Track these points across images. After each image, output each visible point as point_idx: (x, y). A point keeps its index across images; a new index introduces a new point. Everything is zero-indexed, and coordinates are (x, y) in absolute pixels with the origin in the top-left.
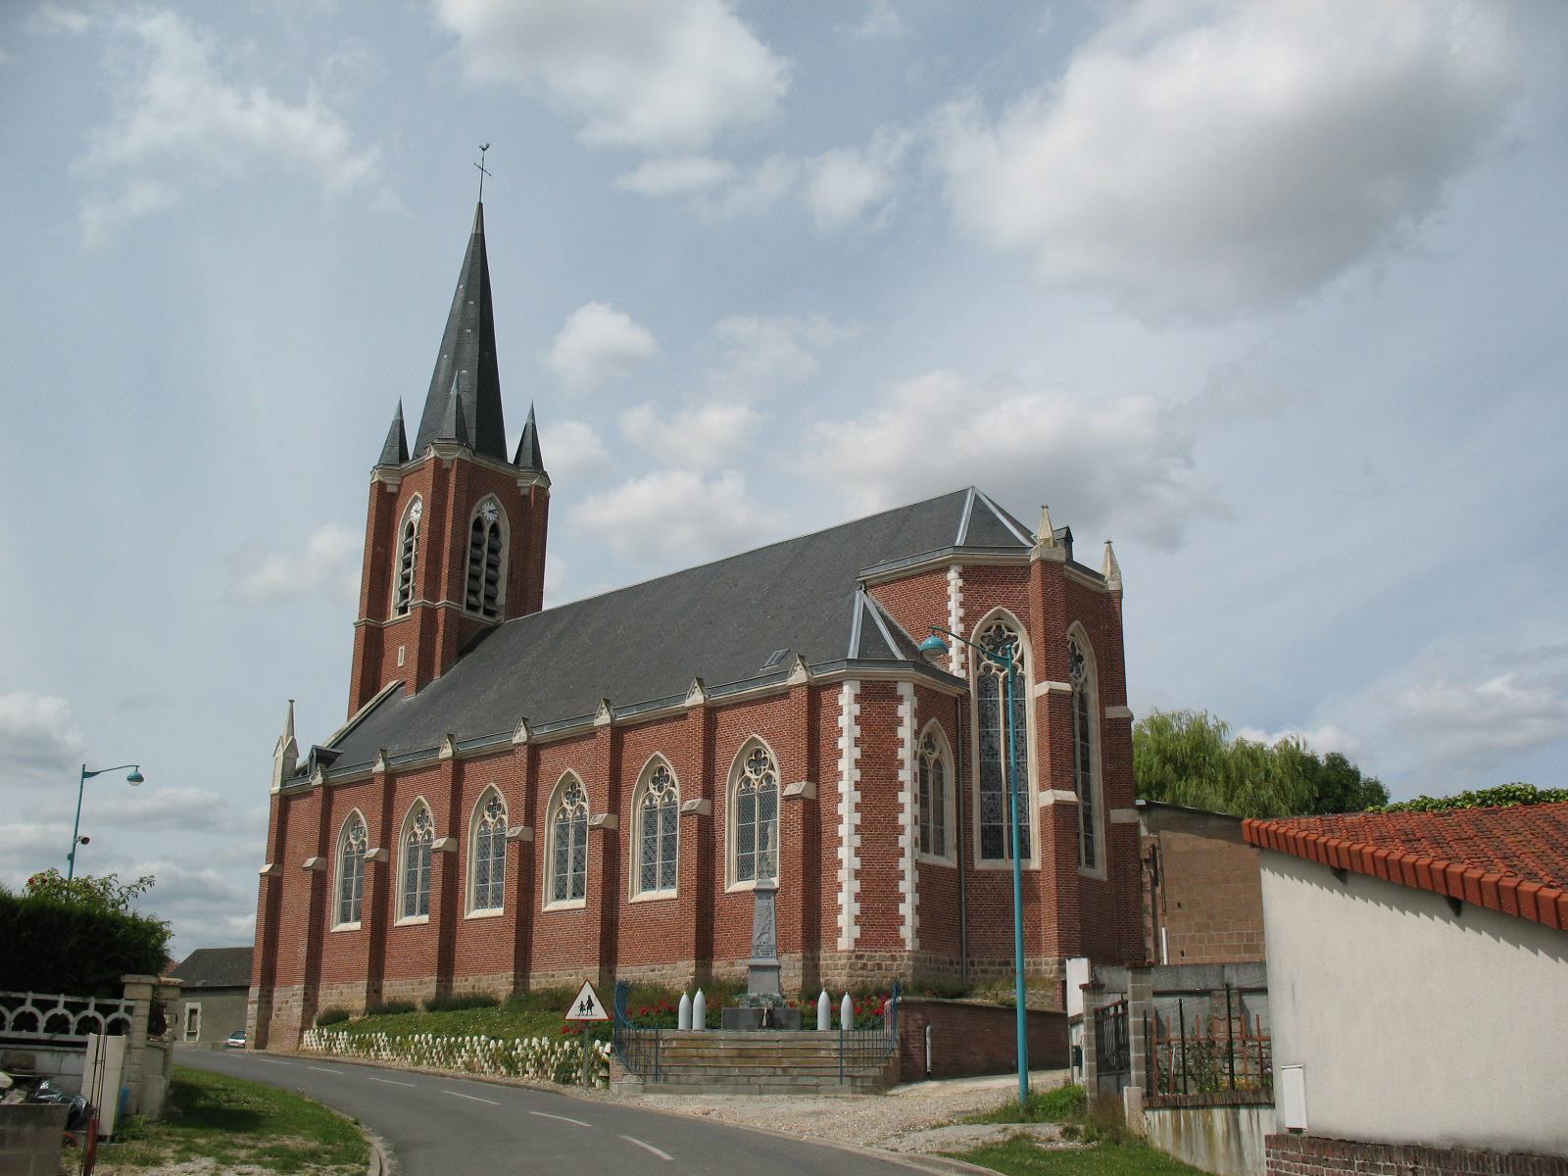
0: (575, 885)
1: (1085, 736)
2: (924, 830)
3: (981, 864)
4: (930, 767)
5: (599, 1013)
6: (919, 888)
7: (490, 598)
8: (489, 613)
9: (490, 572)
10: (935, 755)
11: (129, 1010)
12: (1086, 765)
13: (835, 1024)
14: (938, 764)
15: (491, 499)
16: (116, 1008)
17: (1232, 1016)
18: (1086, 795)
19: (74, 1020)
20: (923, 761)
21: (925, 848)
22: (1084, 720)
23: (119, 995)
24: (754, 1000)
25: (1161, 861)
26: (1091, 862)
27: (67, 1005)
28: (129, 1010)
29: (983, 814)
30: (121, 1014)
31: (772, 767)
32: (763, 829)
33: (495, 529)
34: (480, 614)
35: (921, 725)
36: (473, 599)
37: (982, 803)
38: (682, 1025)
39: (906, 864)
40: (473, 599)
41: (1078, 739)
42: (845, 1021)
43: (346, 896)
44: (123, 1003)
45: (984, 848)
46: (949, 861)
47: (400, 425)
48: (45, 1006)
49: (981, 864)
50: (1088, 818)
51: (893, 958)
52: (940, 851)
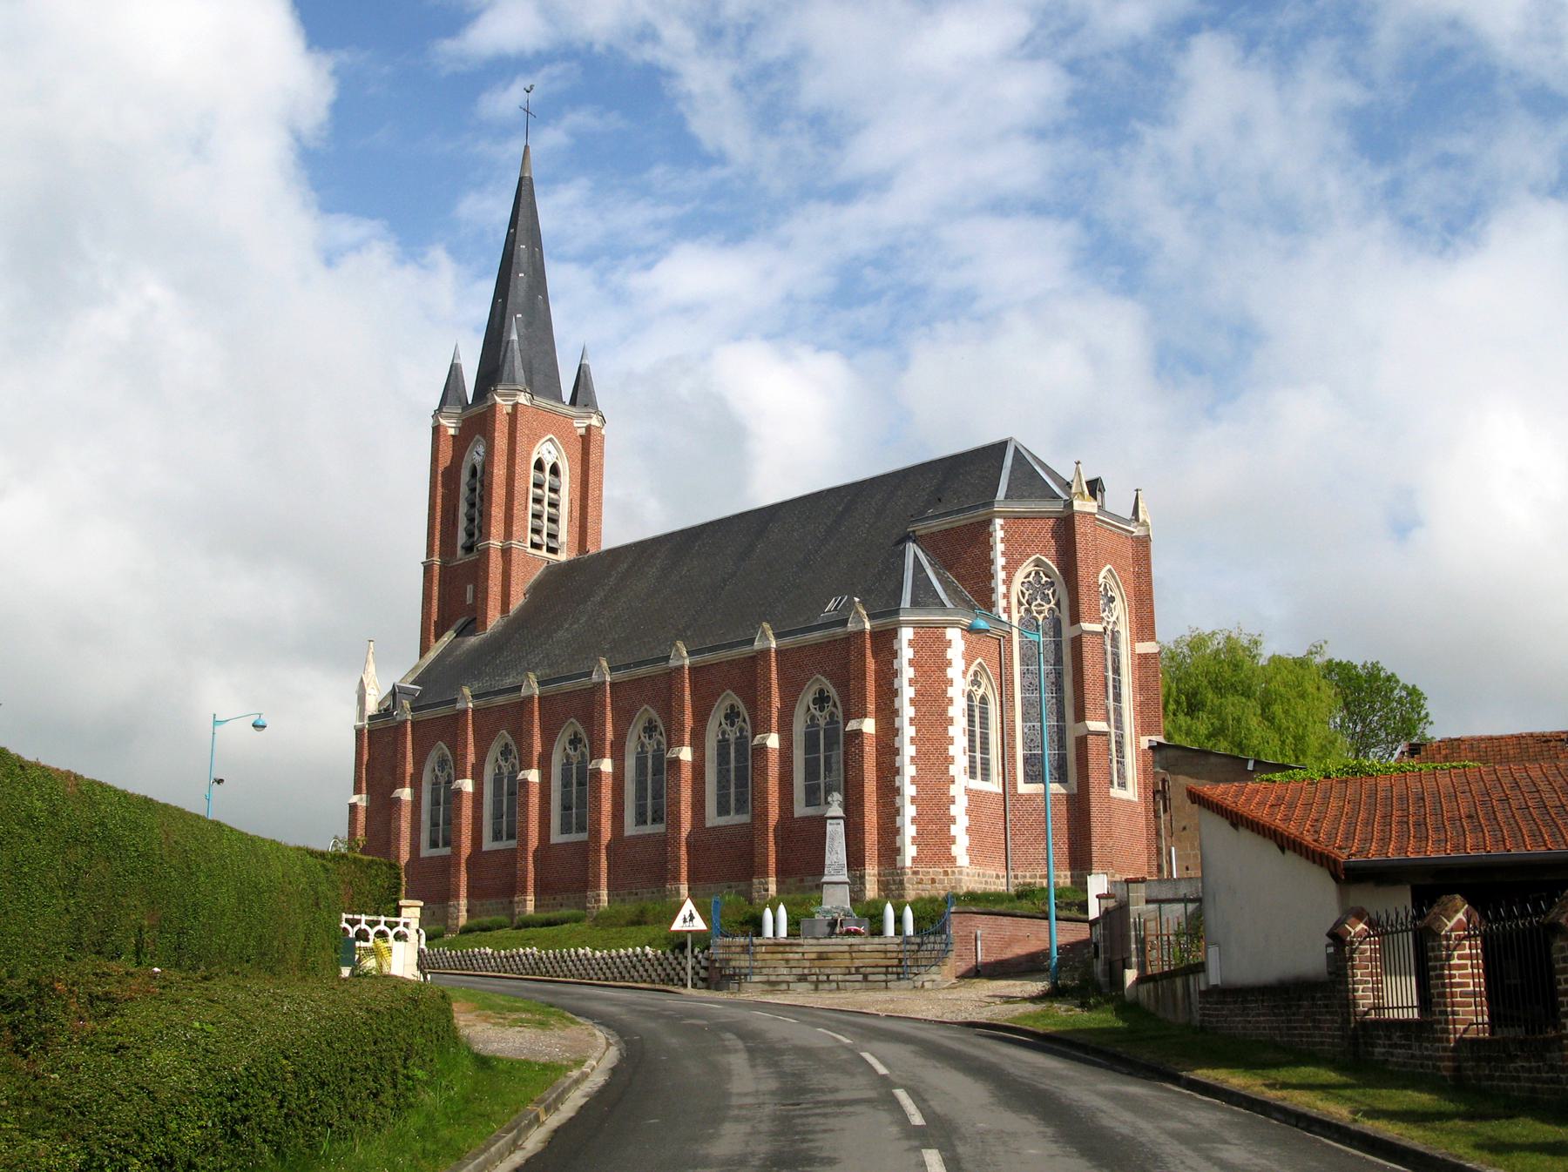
0: (655, 812)
1: (1117, 671)
2: (972, 760)
3: (1024, 788)
4: (976, 703)
5: (699, 924)
6: (969, 812)
7: (552, 536)
8: (552, 550)
9: (553, 511)
10: (981, 692)
11: (406, 925)
12: (1118, 697)
13: (899, 930)
14: (984, 700)
15: (550, 440)
16: (397, 924)
17: (1166, 907)
18: (1119, 725)
19: (372, 932)
20: (970, 698)
21: (973, 775)
22: (1116, 656)
23: (398, 915)
24: (828, 912)
25: (746, 1095)
26: (1123, 785)
27: (367, 923)
28: (406, 925)
29: (1024, 743)
30: (401, 928)
31: (835, 705)
32: (827, 759)
33: (555, 470)
34: (544, 552)
35: (968, 665)
36: (536, 539)
37: (1024, 733)
38: (768, 931)
39: (956, 790)
40: (536, 539)
41: (1110, 673)
42: (909, 929)
43: (435, 824)
44: (401, 920)
45: (1026, 774)
46: (994, 786)
47: (455, 372)
48: (372, 924)
49: (1024, 788)
50: (1120, 744)
51: (946, 873)
52: (986, 776)
